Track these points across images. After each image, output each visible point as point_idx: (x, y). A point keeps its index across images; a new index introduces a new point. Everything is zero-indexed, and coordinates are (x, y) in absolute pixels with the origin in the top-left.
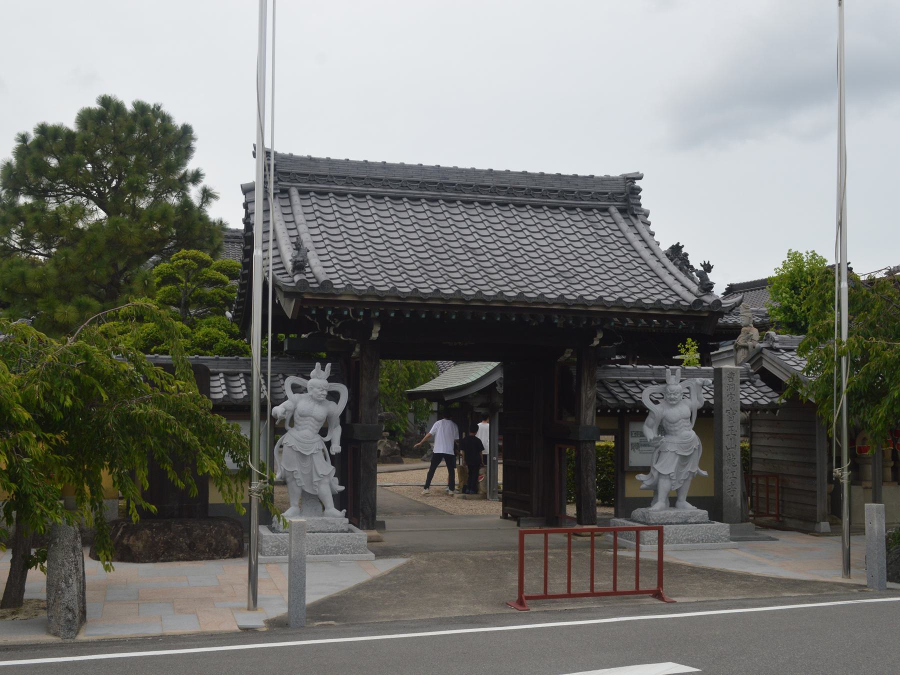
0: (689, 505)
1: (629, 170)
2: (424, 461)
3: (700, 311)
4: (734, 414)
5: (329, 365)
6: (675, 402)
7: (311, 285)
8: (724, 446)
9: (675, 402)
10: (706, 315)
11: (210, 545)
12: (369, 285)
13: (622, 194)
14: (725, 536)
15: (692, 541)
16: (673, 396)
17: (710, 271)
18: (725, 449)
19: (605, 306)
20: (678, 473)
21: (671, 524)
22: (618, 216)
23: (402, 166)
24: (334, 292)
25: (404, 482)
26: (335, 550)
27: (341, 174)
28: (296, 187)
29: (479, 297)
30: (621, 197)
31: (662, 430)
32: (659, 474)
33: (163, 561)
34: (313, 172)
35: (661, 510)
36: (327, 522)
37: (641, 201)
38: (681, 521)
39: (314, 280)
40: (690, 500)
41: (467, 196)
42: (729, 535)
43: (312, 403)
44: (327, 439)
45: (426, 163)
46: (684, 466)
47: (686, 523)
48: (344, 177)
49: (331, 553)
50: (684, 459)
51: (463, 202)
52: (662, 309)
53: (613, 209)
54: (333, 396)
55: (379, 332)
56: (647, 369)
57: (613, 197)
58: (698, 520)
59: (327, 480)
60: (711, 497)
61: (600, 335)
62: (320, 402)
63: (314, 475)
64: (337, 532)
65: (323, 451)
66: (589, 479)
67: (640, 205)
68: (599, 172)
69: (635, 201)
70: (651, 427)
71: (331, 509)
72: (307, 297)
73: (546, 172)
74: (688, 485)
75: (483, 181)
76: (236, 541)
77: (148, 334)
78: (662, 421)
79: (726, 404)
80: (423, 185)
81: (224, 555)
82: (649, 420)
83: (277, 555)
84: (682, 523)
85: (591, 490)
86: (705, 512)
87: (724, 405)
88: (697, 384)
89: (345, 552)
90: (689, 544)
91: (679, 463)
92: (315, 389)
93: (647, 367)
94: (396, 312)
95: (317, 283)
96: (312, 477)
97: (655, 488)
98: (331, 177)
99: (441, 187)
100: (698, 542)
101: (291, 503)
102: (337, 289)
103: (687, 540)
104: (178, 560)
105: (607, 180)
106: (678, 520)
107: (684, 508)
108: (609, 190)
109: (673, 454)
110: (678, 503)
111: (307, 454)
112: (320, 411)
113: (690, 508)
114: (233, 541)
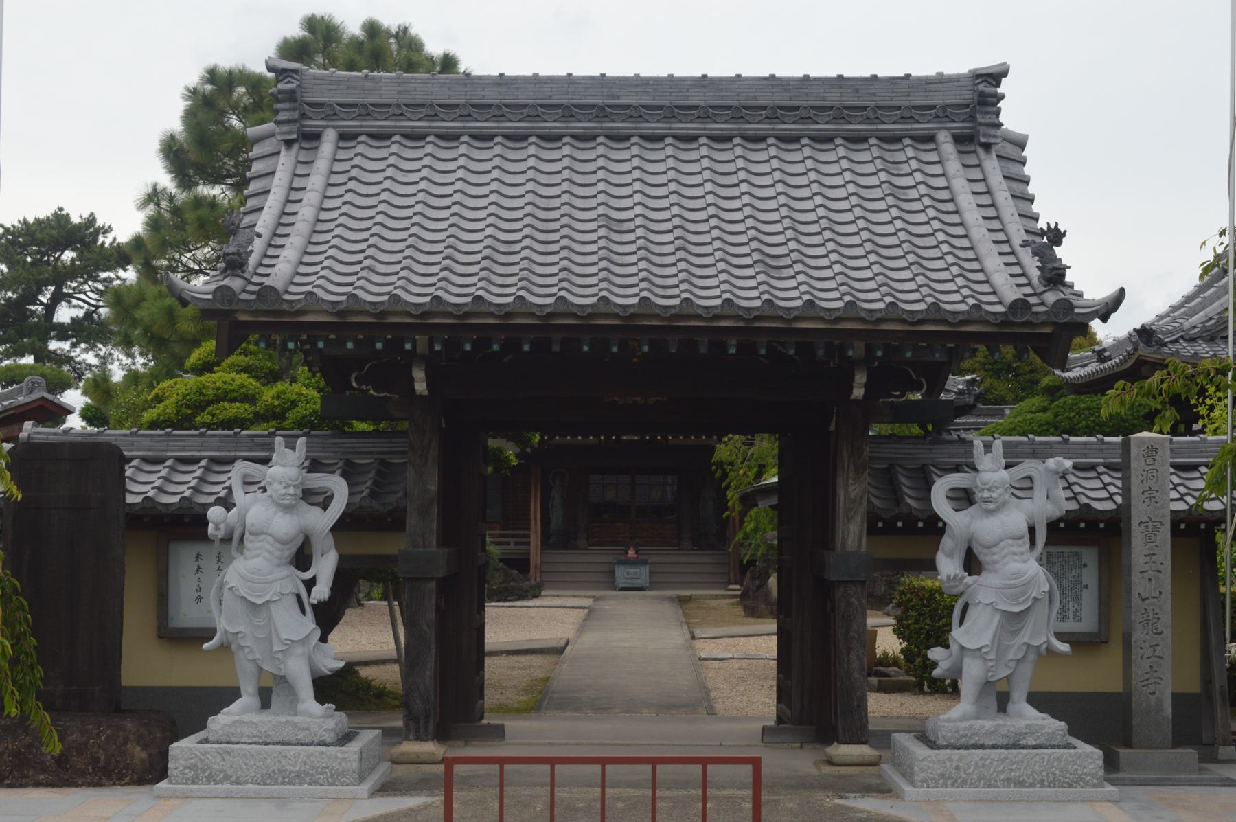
0: (1031, 711)
1: (985, 61)
2: (888, 615)
3: (1028, 324)
4: (1156, 529)
5: (301, 441)
6: (991, 507)
7: (1035, 309)
8: (1135, 593)
9: (991, 507)
10: (1048, 330)
11: (96, 760)
12: (971, 301)
13: (967, 106)
14: (1094, 775)
15: (1020, 783)
16: (986, 494)
17: (1059, 243)
18: (1136, 601)
19: (944, 322)
20: (999, 645)
21: (983, 747)
22: (948, 147)
23: (536, 80)
24: (285, 307)
25: (753, 653)
26: (298, 778)
27: (419, 100)
28: (334, 127)
29: (976, 315)
30: (966, 113)
31: (972, 564)
32: (962, 648)
33: (10, 786)
34: (367, 100)
35: (964, 718)
36: (295, 726)
37: (1002, 119)
38: (1005, 742)
39: (992, 298)
40: (1039, 700)
41: (720, 127)
42: (1101, 773)
43: (272, 509)
44: (308, 575)
45: (578, 72)
46: (1016, 633)
47: (1015, 746)
48: (423, 106)
49: (290, 783)
50: (1014, 620)
51: (780, 139)
52: (944, 322)
53: (944, 138)
54: (316, 498)
55: (866, 386)
56: (1022, 443)
57: (943, 114)
58: (1042, 741)
59: (299, 650)
60: (1118, 694)
61: (860, 378)
62: (288, 509)
63: (275, 640)
64: (311, 744)
65: (298, 597)
66: (853, 656)
67: (1000, 125)
68: (923, 68)
69: (992, 119)
70: (950, 555)
71: (308, 702)
72: (243, 318)
73: (813, 74)
74: (1026, 671)
75: (687, 98)
76: (144, 755)
77: (185, 396)
78: (970, 541)
79: (1139, 513)
80: (568, 112)
81: (120, 779)
82: (946, 542)
83: (194, 783)
84: (1006, 747)
85: (856, 676)
86: (1063, 723)
87: (1133, 512)
88: (1047, 469)
89: (316, 782)
90: (1012, 790)
91: (1001, 627)
92: (276, 485)
93: (1093, 439)
94: (387, 343)
95: (1000, 303)
96: (271, 644)
97: (956, 672)
98: (398, 106)
99: (601, 112)
100: (1032, 785)
101: (243, 693)
102: (1037, 313)
103: (1008, 781)
104: (37, 784)
105: (941, 81)
106: (1000, 741)
107: (1020, 716)
108: (937, 99)
109: (989, 609)
110: (1011, 707)
111: (259, 601)
112: (285, 525)
113: (1026, 717)
114: (139, 754)
